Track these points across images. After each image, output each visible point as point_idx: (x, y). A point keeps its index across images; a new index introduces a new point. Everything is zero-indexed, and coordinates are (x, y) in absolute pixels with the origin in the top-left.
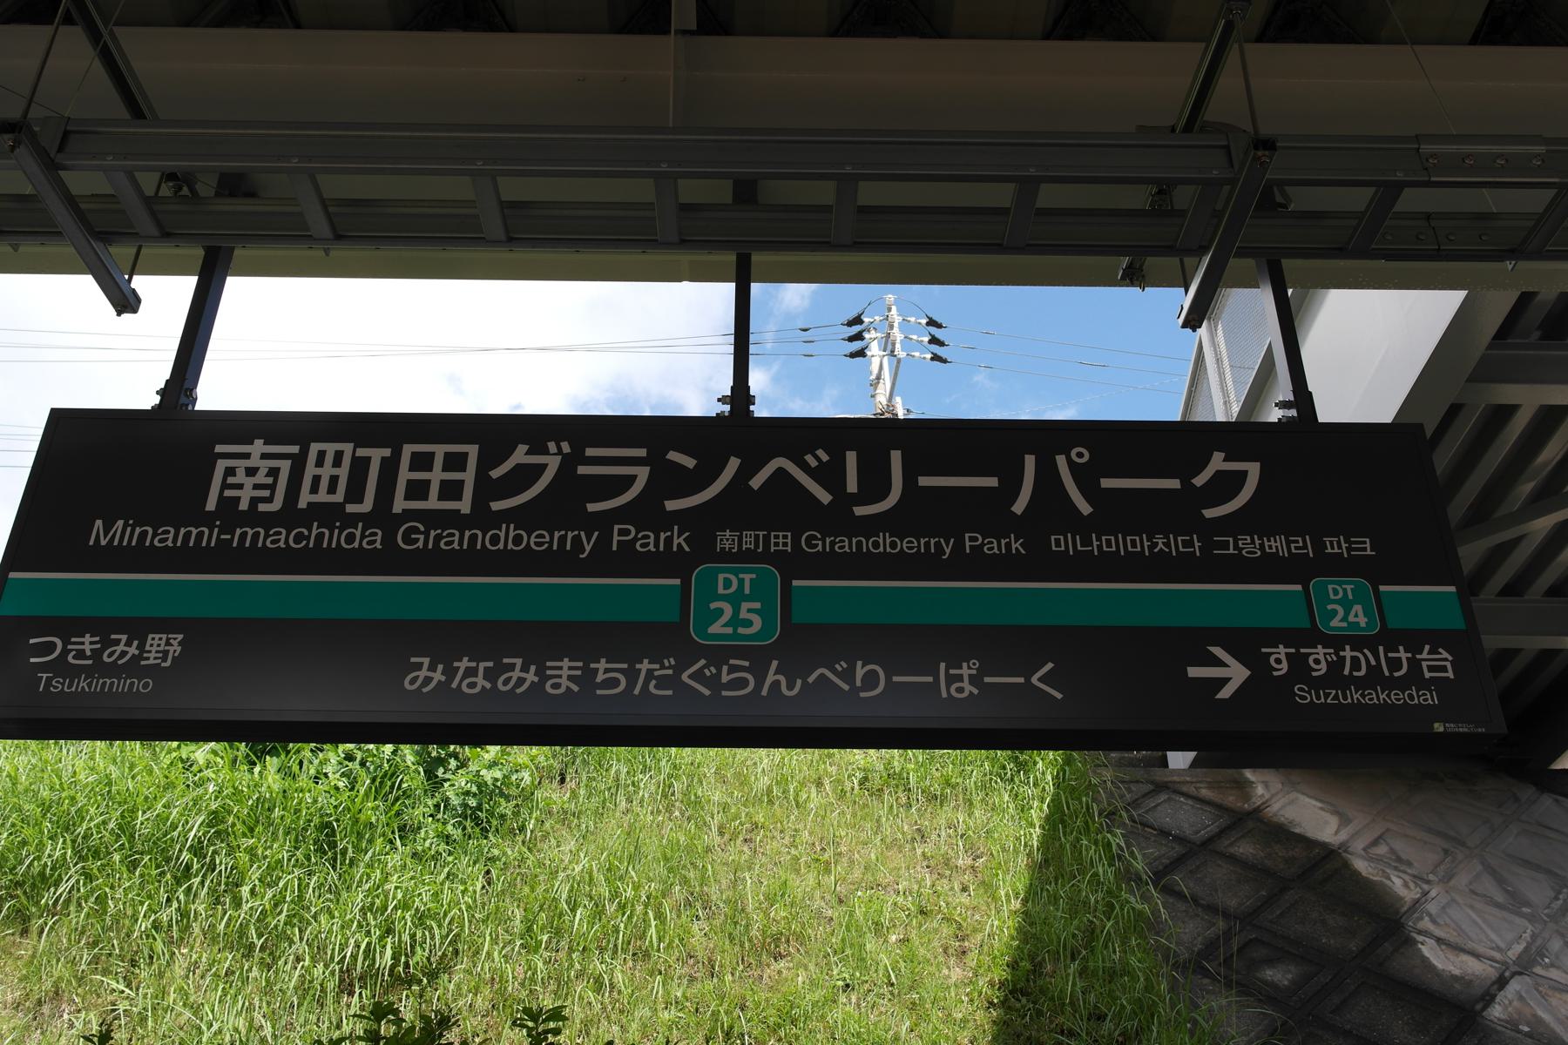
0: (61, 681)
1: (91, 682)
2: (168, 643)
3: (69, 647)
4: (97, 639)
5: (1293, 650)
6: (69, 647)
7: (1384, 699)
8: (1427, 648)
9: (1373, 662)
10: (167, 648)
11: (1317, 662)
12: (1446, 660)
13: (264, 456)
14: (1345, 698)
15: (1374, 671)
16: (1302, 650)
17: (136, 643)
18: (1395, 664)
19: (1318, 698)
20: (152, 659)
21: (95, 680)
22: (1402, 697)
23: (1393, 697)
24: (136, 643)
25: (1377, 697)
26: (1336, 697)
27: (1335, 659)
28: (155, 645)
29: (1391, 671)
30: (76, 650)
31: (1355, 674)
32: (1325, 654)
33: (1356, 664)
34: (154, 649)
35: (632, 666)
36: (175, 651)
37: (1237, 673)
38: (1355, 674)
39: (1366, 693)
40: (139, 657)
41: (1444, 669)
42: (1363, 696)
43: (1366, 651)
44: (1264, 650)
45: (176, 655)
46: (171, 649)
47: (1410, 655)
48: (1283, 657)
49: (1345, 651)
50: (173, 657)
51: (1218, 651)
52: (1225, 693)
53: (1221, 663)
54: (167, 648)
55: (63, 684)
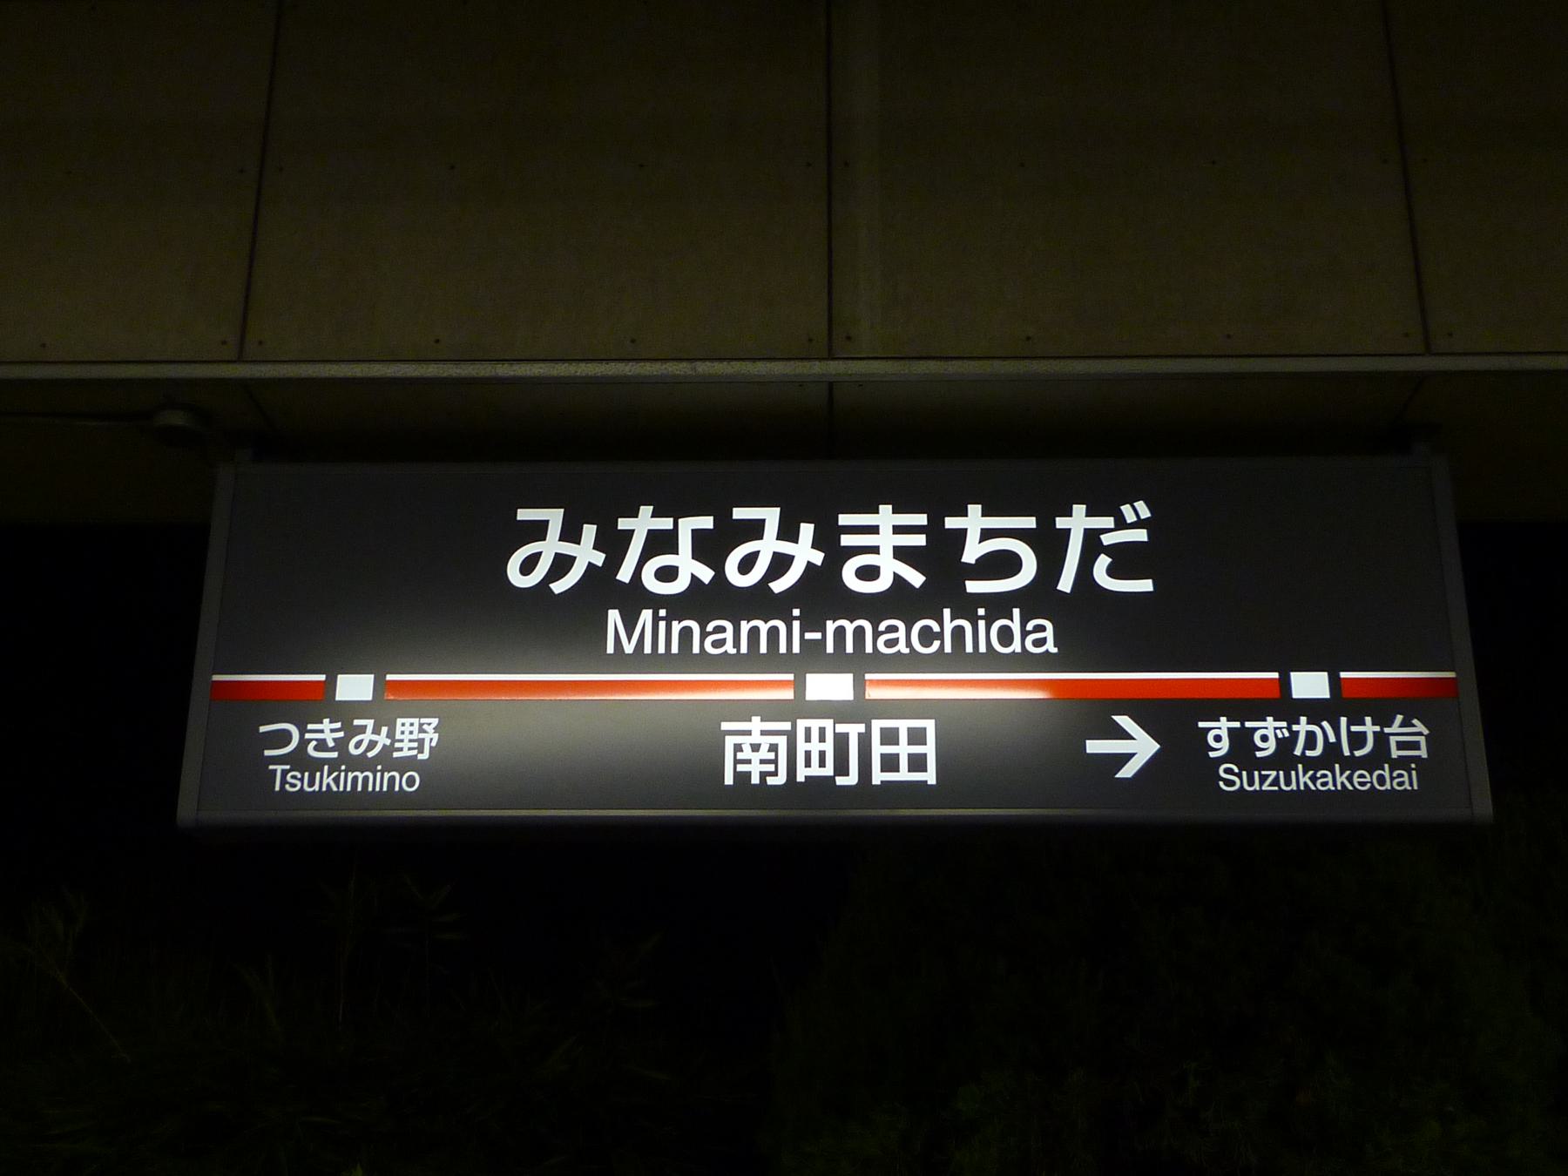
0: (299, 776)
1: (339, 776)
2: (421, 730)
3: (307, 736)
4: (338, 725)
5: (1237, 724)
6: (307, 736)
7: (1342, 783)
8: (1399, 718)
9: (1332, 739)
10: (422, 736)
11: (1264, 738)
12: (1420, 734)
13: (764, 733)
14: (1288, 783)
15: (1332, 750)
16: (1248, 724)
17: (384, 730)
18: (1357, 740)
19: (1251, 783)
20: (405, 751)
21: (343, 774)
22: (1369, 780)
23: (1356, 780)
24: (384, 730)
25: (1334, 780)
26: (1276, 782)
27: (1287, 734)
28: (407, 733)
29: (1351, 750)
30: (316, 740)
31: (1308, 753)
32: (1276, 728)
33: (1311, 740)
34: (406, 737)
35: (1046, 523)
36: (431, 739)
37: (1141, 747)
38: (1308, 753)
39: (1318, 775)
40: (388, 750)
41: (1415, 746)
42: (1314, 779)
43: (1325, 724)
44: (1201, 725)
45: (434, 744)
46: (427, 737)
47: (1377, 728)
48: (1224, 734)
49: (1298, 723)
50: (431, 747)
51: (1124, 721)
52: (1127, 772)
53: (1126, 736)
54: (422, 736)
55: (302, 780)
